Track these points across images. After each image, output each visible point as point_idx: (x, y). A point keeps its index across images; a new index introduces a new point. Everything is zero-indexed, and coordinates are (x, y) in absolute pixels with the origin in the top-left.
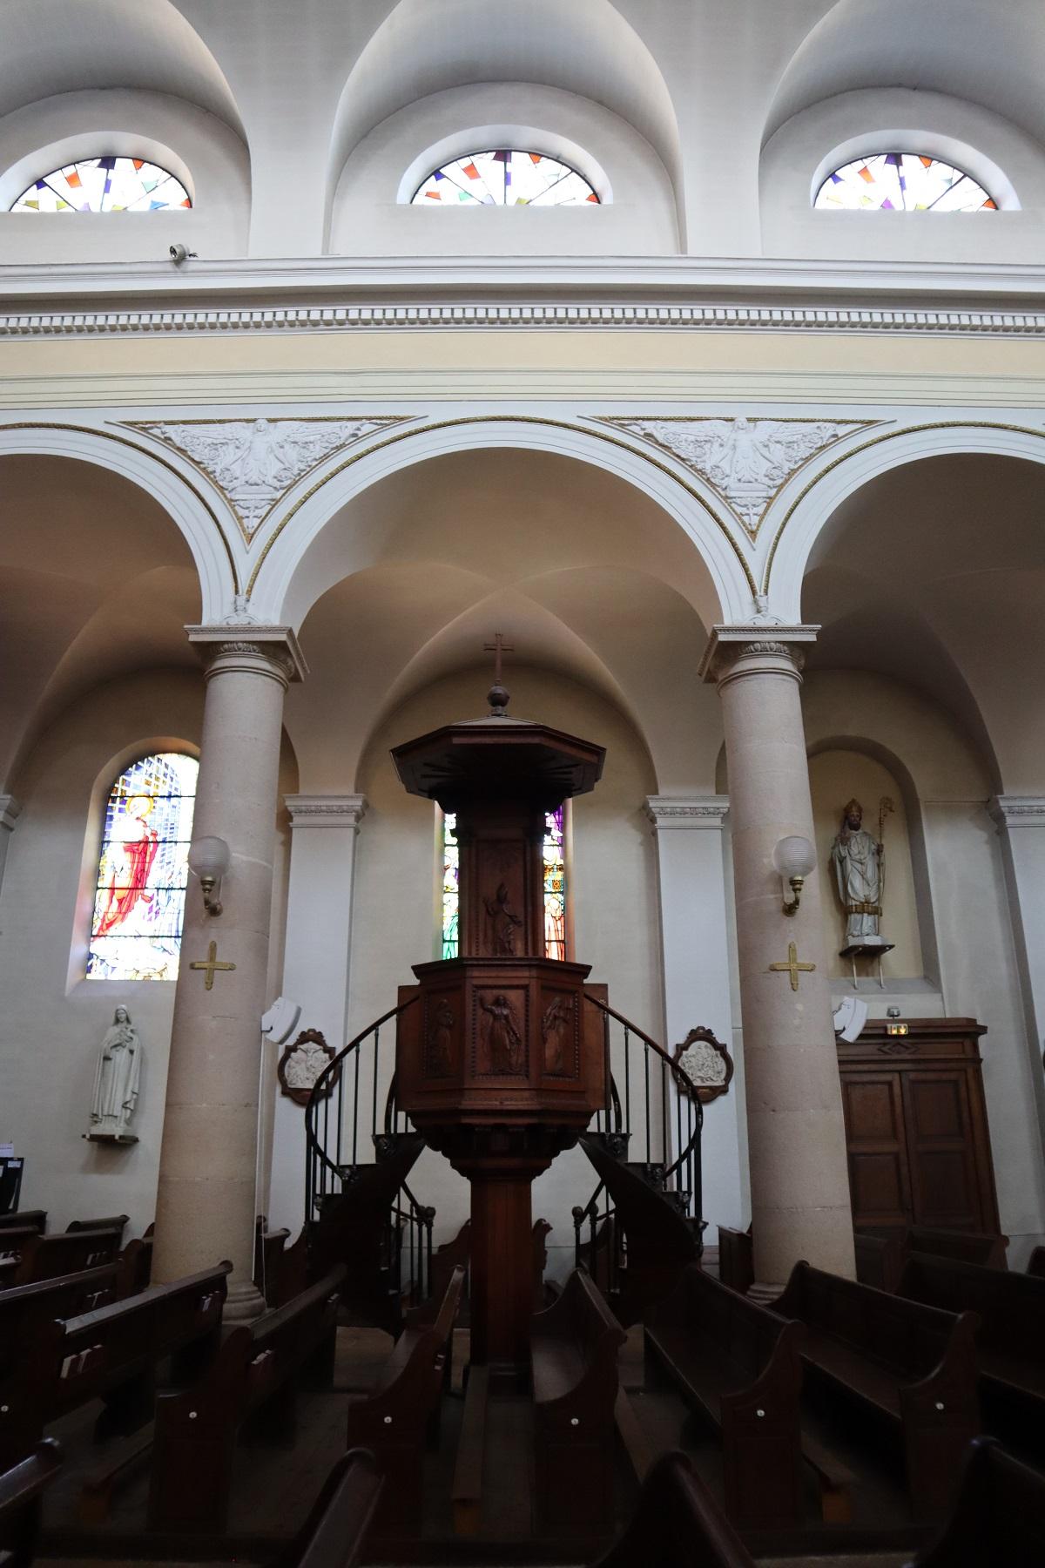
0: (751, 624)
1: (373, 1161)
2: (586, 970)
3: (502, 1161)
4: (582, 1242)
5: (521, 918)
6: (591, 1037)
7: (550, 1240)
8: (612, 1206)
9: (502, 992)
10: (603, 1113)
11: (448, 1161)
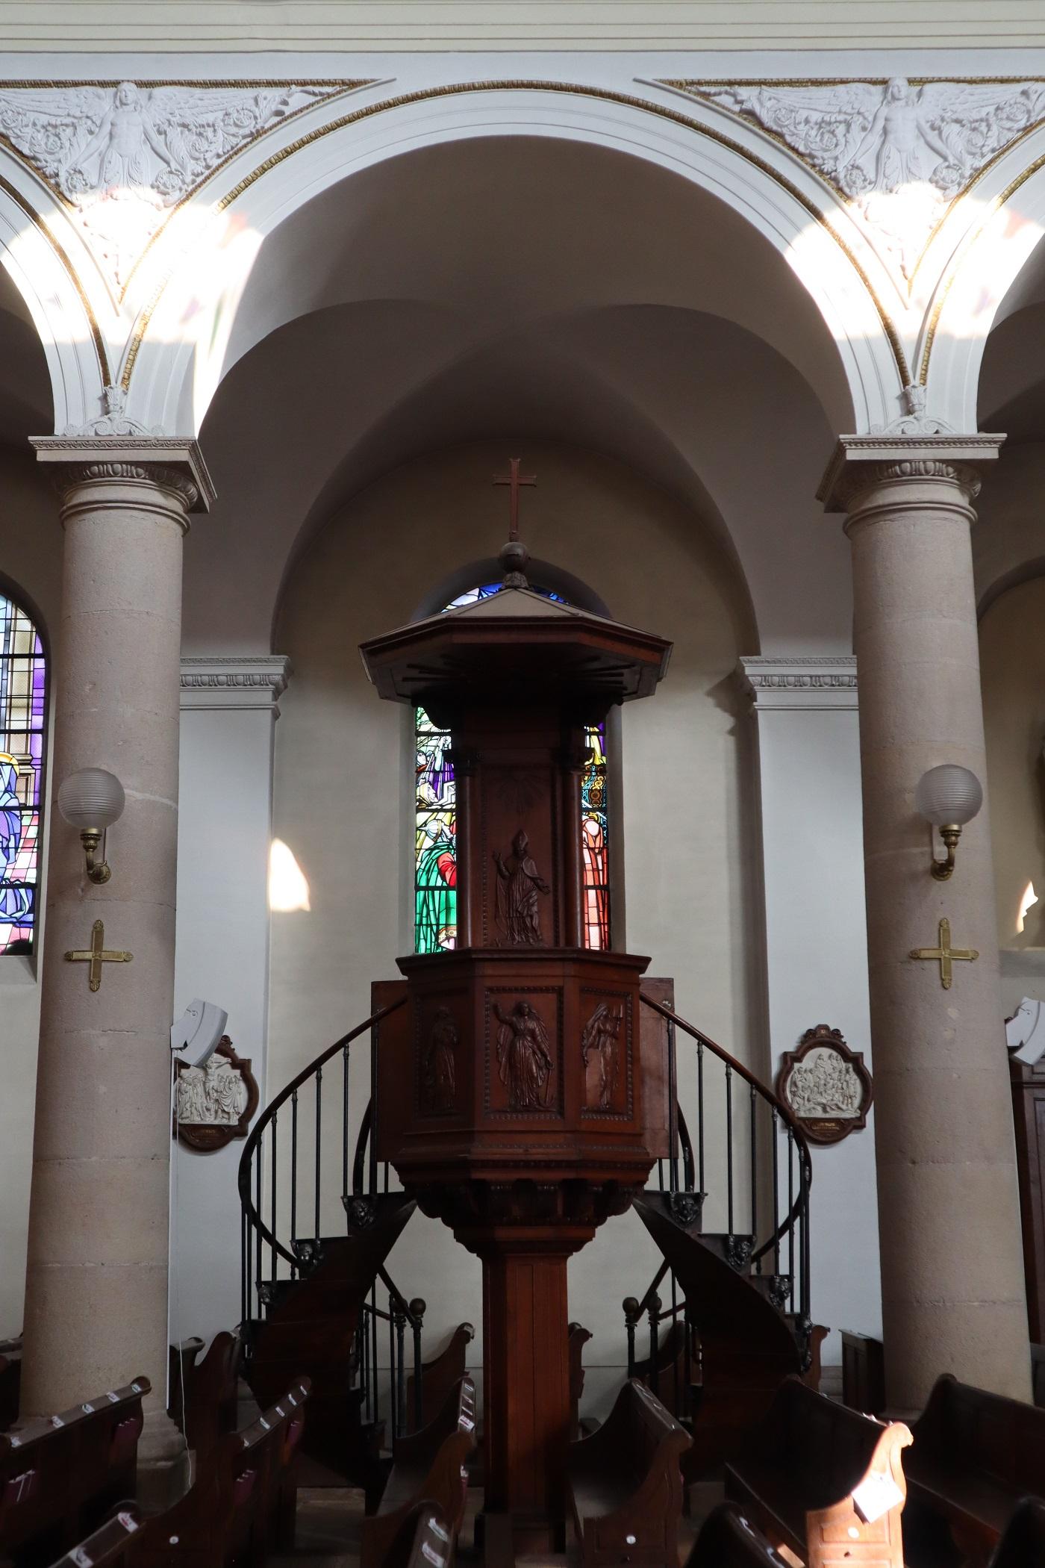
0: (898, 434)
1: (343, 1232)
2: (643, 962)
3: (524, 1229)
4: (637, 1359)
5: (549, 882)
6: (649, 1053)
7: (590, 1352)
8: (681, 1298)
9: (526, 996)
10: (666, 1163)
11: (450, 1231)
